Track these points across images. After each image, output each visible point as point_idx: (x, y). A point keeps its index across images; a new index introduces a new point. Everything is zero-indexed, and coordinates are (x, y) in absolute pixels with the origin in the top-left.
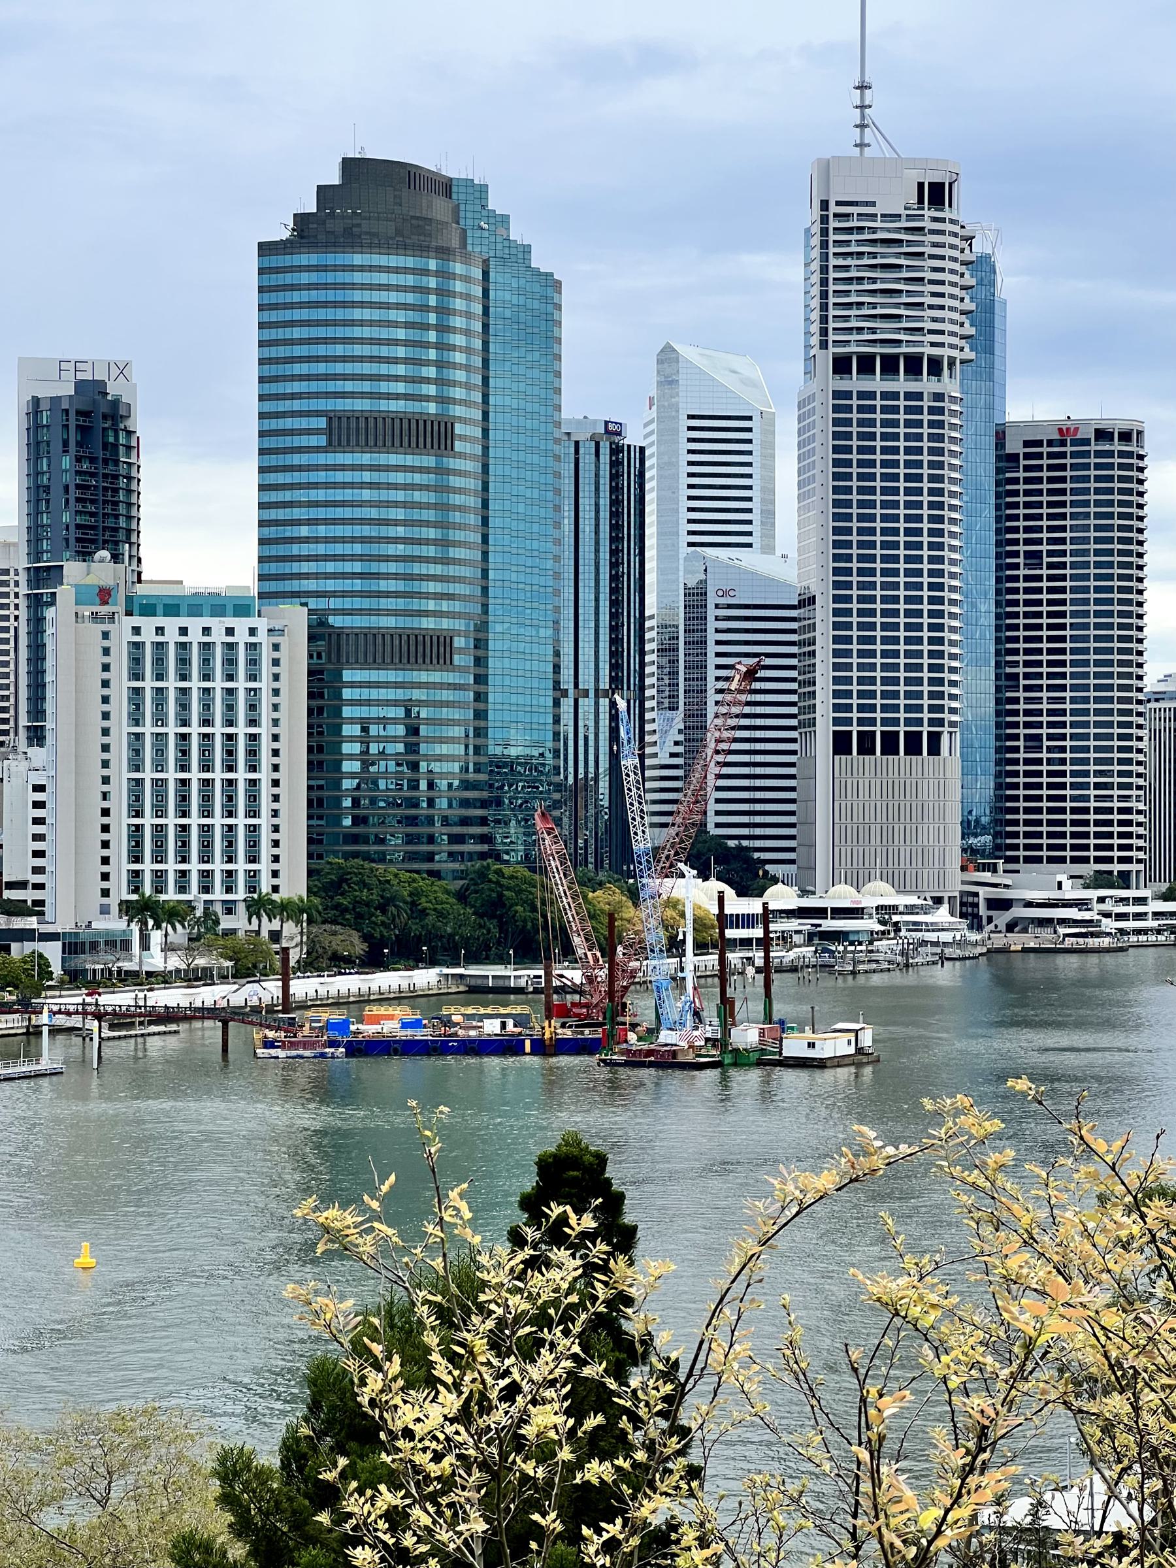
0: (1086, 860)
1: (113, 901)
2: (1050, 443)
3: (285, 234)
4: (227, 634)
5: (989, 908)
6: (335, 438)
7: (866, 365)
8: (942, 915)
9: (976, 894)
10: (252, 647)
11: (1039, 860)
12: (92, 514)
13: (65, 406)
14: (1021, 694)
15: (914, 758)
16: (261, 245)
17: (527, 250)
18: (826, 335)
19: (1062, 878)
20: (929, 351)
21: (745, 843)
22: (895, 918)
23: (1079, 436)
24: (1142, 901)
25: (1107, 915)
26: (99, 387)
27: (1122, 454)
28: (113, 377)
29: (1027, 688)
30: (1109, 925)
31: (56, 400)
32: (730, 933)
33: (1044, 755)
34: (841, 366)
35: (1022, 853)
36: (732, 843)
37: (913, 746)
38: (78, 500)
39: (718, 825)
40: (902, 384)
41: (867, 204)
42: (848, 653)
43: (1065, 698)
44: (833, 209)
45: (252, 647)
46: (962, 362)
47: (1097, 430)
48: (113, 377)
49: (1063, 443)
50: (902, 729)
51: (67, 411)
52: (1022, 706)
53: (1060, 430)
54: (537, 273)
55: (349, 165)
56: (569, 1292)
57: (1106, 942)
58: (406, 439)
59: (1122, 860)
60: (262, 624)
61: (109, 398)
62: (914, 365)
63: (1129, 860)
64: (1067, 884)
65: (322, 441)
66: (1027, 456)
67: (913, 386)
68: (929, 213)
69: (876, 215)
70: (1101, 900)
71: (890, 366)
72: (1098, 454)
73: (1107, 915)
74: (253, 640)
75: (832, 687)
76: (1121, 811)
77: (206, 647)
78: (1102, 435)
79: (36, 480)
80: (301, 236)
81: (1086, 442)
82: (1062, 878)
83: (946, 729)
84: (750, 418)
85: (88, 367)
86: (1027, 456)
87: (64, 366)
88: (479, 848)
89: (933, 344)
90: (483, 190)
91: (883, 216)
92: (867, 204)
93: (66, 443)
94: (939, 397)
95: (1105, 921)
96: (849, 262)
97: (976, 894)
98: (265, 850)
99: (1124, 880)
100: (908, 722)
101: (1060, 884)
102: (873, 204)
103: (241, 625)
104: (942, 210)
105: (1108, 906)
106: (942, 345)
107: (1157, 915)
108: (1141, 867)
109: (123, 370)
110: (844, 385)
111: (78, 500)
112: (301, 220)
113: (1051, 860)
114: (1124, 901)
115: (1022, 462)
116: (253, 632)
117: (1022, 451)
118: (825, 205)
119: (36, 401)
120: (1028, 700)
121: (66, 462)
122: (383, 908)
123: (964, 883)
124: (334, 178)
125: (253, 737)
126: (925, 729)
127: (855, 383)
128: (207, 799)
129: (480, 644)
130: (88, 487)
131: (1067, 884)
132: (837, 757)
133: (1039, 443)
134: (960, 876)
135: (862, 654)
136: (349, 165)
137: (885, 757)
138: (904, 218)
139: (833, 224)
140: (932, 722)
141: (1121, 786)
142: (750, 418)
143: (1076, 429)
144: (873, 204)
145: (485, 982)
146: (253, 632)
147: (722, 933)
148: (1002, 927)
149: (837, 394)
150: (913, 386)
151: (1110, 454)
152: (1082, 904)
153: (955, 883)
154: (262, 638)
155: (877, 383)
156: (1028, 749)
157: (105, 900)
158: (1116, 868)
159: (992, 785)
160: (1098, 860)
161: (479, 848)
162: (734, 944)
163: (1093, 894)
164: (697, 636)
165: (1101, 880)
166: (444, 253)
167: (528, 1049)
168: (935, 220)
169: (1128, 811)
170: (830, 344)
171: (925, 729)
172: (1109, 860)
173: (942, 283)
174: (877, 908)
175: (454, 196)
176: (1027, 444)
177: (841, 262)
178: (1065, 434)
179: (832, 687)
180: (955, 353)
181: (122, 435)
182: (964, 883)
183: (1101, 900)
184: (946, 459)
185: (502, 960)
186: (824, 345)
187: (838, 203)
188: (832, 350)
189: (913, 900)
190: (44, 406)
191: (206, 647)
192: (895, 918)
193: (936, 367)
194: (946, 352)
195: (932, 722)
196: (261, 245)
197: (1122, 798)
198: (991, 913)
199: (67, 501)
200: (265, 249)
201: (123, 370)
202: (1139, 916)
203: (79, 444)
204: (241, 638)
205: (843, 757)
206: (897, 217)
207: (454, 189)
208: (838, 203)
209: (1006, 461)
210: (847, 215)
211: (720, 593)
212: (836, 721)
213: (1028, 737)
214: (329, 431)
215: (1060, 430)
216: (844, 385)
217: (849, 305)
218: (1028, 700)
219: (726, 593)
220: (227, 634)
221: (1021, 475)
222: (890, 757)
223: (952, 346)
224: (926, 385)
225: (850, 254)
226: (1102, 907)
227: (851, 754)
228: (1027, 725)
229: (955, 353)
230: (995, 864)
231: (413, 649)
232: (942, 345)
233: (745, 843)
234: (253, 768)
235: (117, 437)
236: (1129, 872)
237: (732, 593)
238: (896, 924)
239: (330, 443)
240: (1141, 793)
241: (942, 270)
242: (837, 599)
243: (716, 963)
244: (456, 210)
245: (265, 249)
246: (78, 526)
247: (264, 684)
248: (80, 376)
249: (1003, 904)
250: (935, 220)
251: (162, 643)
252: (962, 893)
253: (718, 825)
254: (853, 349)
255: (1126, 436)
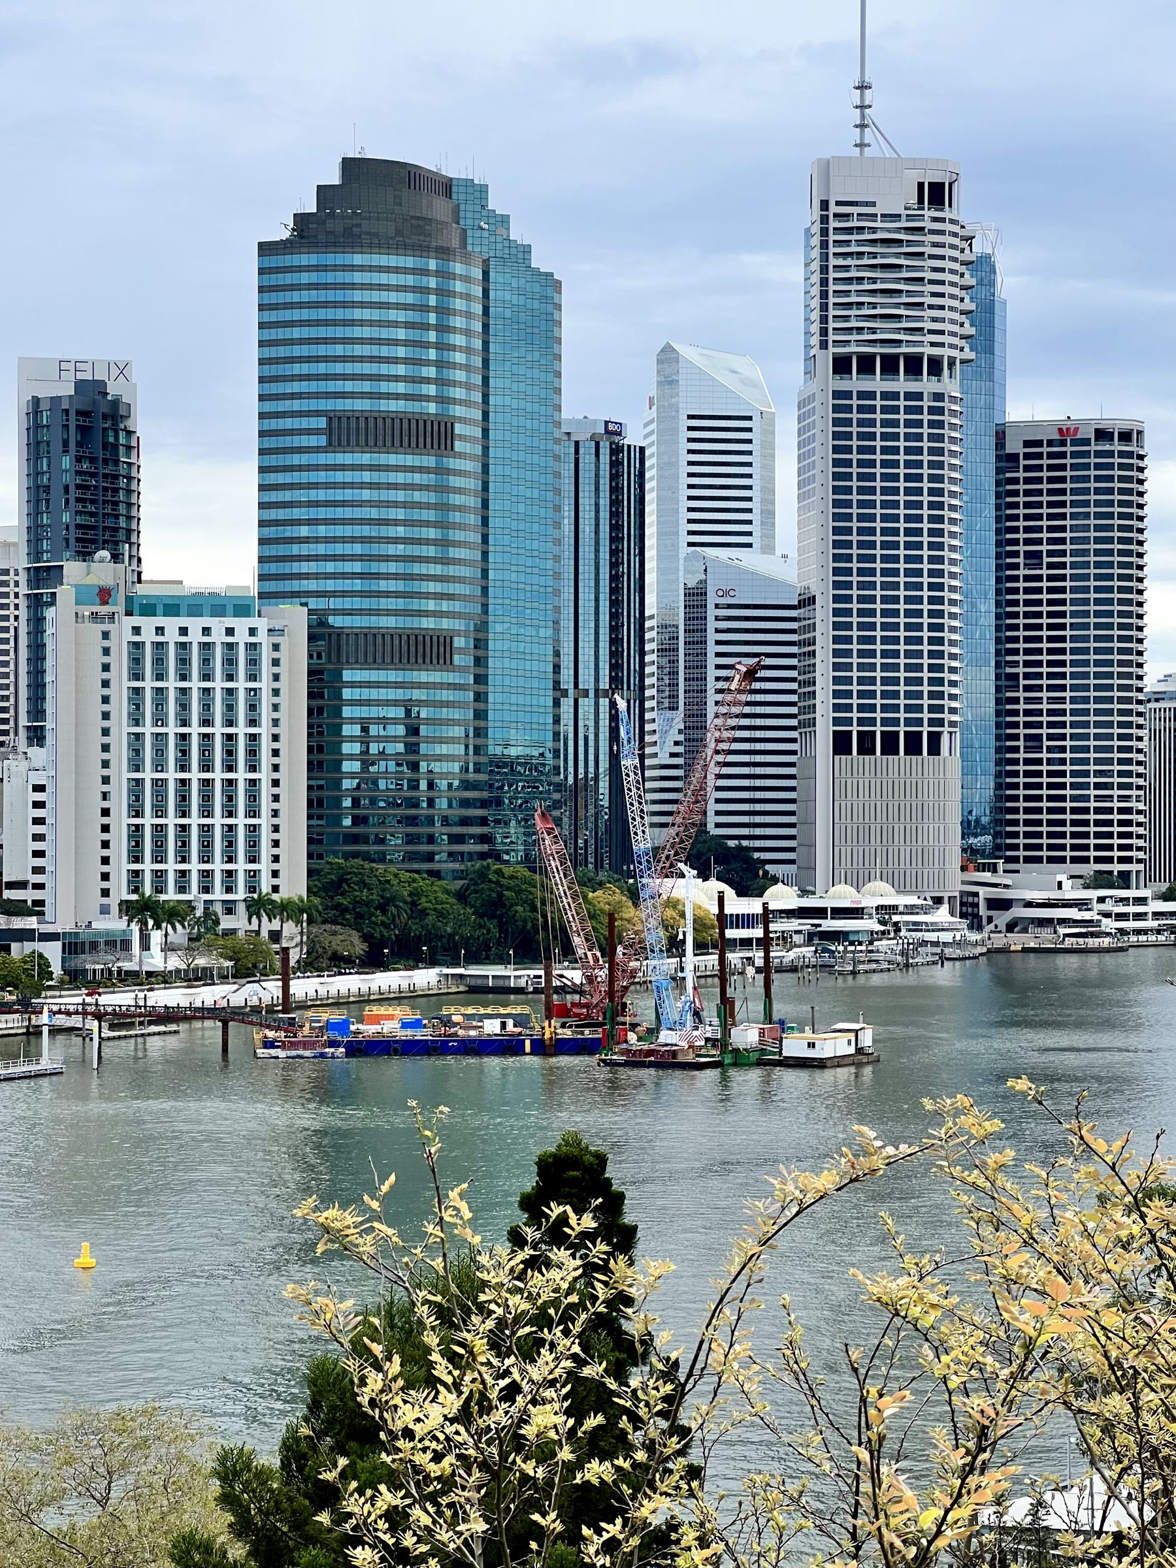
0: (1086, 860)
1: (113, 901)
2: (1050, 443)
3: (285, 234)
4: (227, 634)
5: (989, 908)
6: (335, 438)
7: (866, 365)
8: (942, 915)
9: (976, 894)
10: (252, 647)
11: (1039, 860)
12: (92, 514)
13: (65, 406)
14: (1021, 694)
15: (914, 758)
16: (261, 245)
17: (527, 250)
18: (826, 335)
19: (1062, 878)
20: (929, 351)
21: (745, 843)
22: (895, 918)
23: (1079, 436)
24: (1142, 901)
25: (1107, 915)
26: (99, 387)
27: (1122, 454)
28: (113, 377)
29: (1027, 688)
30: (1109, 925)
31: (56, 400)
32: (730, 933)
33: (1044, 755)
34: (841, 366)
35: (1022, 853)
36: (732, 843)
37: (913, 746)
38: (78, 500)
39: (718, 825)
40: (902, 384)
41: (867, 204)
42: (848, 653)
43: (1065, 698)
44: (833, 209)
45: (252, 647)
46: (962, 362)
47: (1097, 430)
48: (113, 377)
49: (1063, 443)
50: (902, 729)
51: (67, 411)
52: (1022, 706)
53: (1060, 430)
54: (537, 273)
55: (349, 165)
56: (569, 1292)
57: (1106, 942)
58: (406, 439)
59: (1122, 860)
60: (262, 624)
61: (109, 398)
62: (914, 365)
63: (1129, 860)
64: (1067, 884)
65: (322, 441)
66: (1027, 456)
67: (913, 386)
68: (929, 213)
69: (876, 215)
70: (1101, 900)
71: (890, 366)
72: (1098, 454)
73: (1107, 915)
74: (253, 640)
75: (832, 687)
76: (1121, 811)
77: (206, 647)
78: (1102, 435)
79: (36, 480)
80: (301, 236)
81: (1086, 442)
82: (1062, 878)
83: (946, 729)
84: (750, 418)
85: (88, 367)
86: (1027, 456)
87: (64, 366)
88: (479, 848)
89: (933, 344)
90: (483, 190)
91: (883, 216)
92: (867, 204)
93: (66, 443)
94: (939, 397)
95: (1105, 921)
96: (849, 262)
97: (976, 894)
98: (265, 850)
99: (1124, 880)
100: (908, 722)
101: (1060, 884)
102: (873, 204)
103: (241, 625)
104: (942, 210)
105: (1108, 906)
106: (942, 345)
107: (1157, 915)
108: (1141, 867)
109: (123, 370)
110: (844, 385)
111: (78, 500)
112: (301, 220)
113: (1051, 860)
114: (1124, 901)
115: (1022, 462)
116: (253, 632)
117: (1022, 451)
118: (825, 205)
119: (36, 401)
120: (1028, 700)
121: (66, 462)
122: (383, 908)
123: (964, 883)
124: (334, 178)
125: (253, 737)
126: (925, 729)
127: (855, 383)
128: (207, 799)
129: (480, 644)
130: (88, 487)
131: (1067, 884)
132: (837, 757)
133: (1039, 443)
134: (960, 876)
135: (862, 654)
136: (349, 165)
137: (885, 757)
138: (904, 218)
139: (833, 224)
140: (932, 722)
141: (1121, 786)
142: (750, 418)
143: (1076, 429)
144: (873, 204)
145: (485, 982)
146: (253, 632)
147: (722, 933)
148: (1002, 927)
149: (837, 394)
150: (913, 386)
151: (1110, 454)
152: (1082, 904)
153: (955, 883)
154: (262, 638)
155: (877, 383)
156: (1028, 749)
157: (105, 900)
158: (1116, 868)
159: (992, 785)
160: (1098, 860)
161: (479, 848)
162: (734, 944)
163: (1093, 894)
164: (697, 636)
165: (1101, 880)
166: (444, 253)
167: (528, 1049)
168: (935, 220)
169: (1128, 811)
170: (830, 344)
171: (925, 729)
172: (1109, 860)
173: (942, 283)
174: (877, 908)
175: (454, 196)
176: (1027, 444)
177: (841, 262)
178: (1065, 434)
179: (832, 687)
180: (955, 353)
181: (122, 435)
182: (964, 883)
183: (1101, 900)
184: (946, 459)
185: (502, 960)
186: (824, 345)
187: (838, 203)
188: (832, 350)
189: (913, 900)
190: (44, 406)
191: (206, 647)
192: (895, 918)
193: (936, 367)
194: (946, 352)
195: (932, 722)
196: (261, 245)
197: (1122, 798)
198: (991, 913)
199: (67, 501)
200: (265, 249)
201: (123, 370)
202: (1139, 916)
203: (79, 444)
204: (241, 638)
205: (843, 757)
206: (897, 217)
207: (454, 189)
208: (838, 203)
209: (1006, 461)
210: (847, 215)
211: (720, 593)
212: (836, 721)
213: (1028, 737)
214: (329, 431)
215: (1060, 430)
216: (844, 385)
217: (849, 305)
218: (1028, 700)
219: (726, 593)
220: (227, 634)
221: (1021, 475)
222: (890, 757)
223: (952, 346)
224: (926, 385)
225: (850, 254)
226: (1102, 907)
227: (851, 754)
228: (1027, 725)
229: (955, 353)
230: (995, 864)
231: (413, 649)
232: (942, 345)
233: (745, 843)
234: (253, 768)
235: (117, 437)
236: (1129, 872)
237: (732, 593)
238: (896, 924)
239: (330, 443)
240: (1141, 793)
241: (942, 270)
242: (837, 599)
243: (716, 963)
244: (456, 210)
245: (265, 249)
246: (78, 526)
247: (264, 684)
248: (80, 376)
249: (1003, 904)
250: (935, 220)
251: (162, 643)
252: (962, 893)
253: (718, 825)
254: (853, 349)
255: (1126, 436)
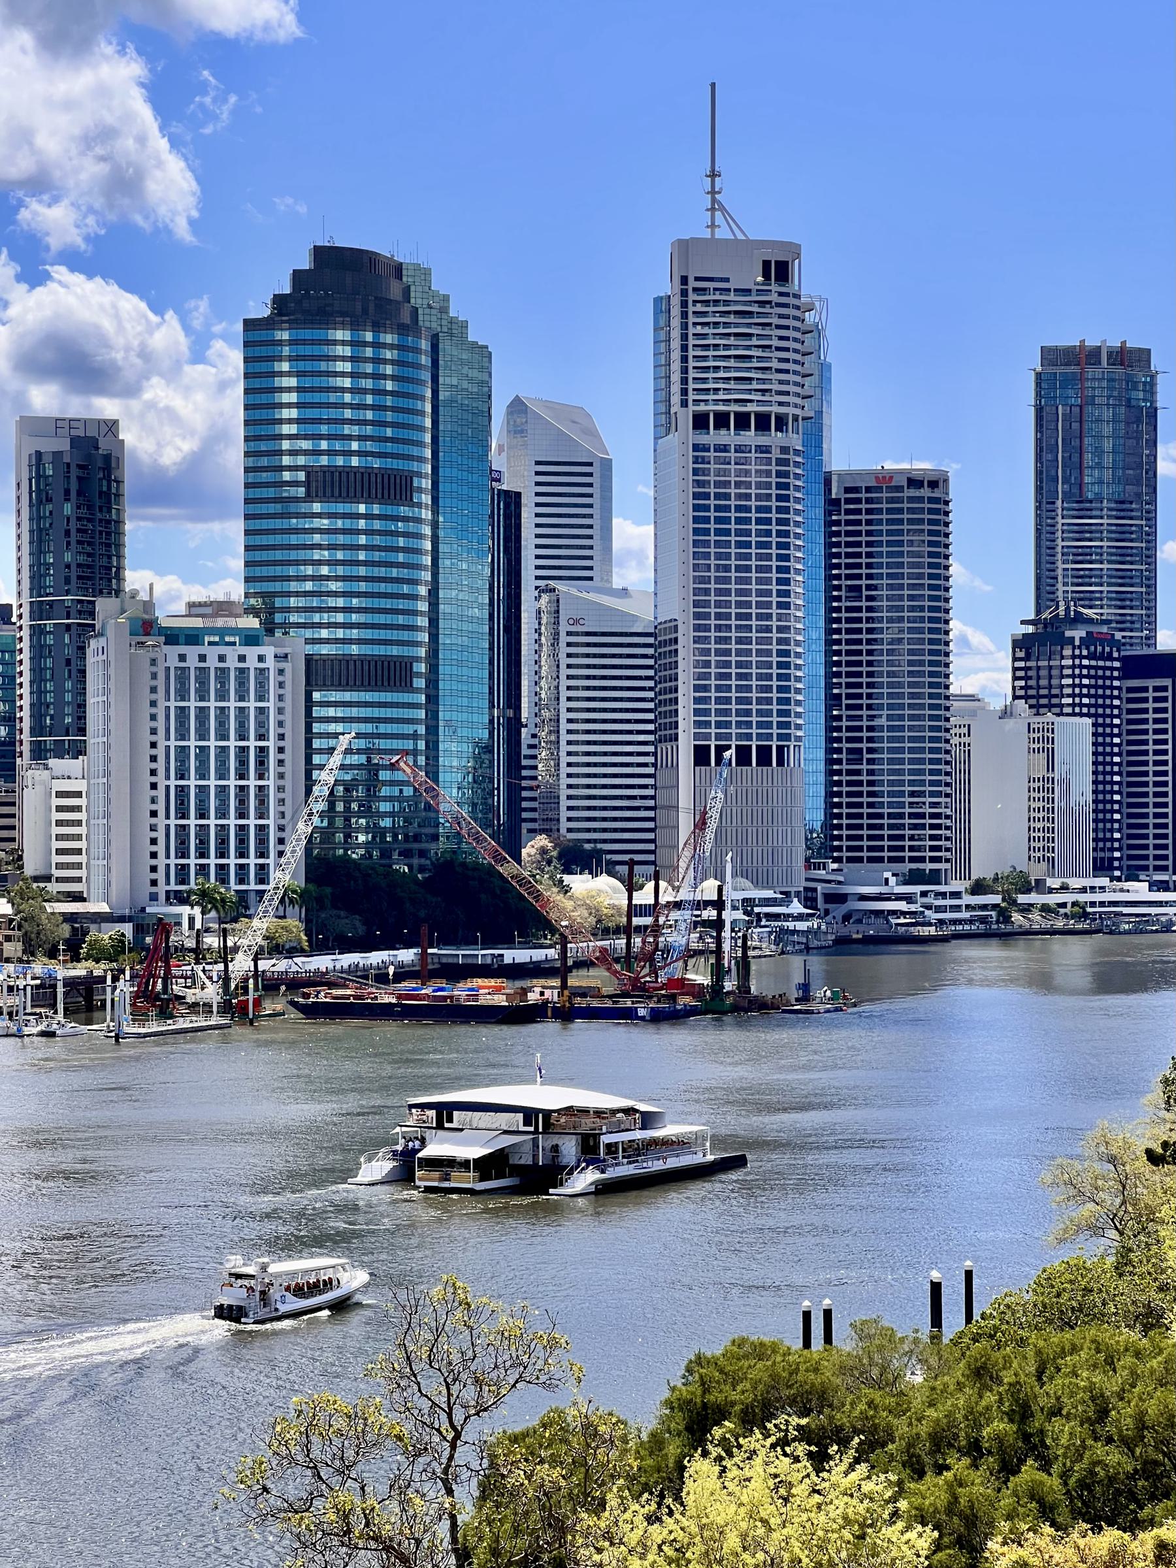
2: (868, 489)
3: (266, 312)
4: (240, 661)
5: (826, 902)
6: (313, 490)
7: (722, 420)
8: (796, 907)
9: (815, 890)
10: (262, 672)
11: (860, 860)
12: (89, 555)
13: (67, 459)
14: (844, 713)
15: (765, 768)
17: (464, 325)
18: (686, 395)
19: (887, 875)
20: (775, 409)
21: (599, 846)
22: (757, 910)
23: (893, 484)
24: (956, 895)
25: (929, 907)
26: (94, 443)
28: (102, 434)
31: (57, 455)
32: (636, 921)
34: (700, 422)
36: (587, 846)
38: (79, 542)
39: (569, 830)
43: (861, 716)
44: (692, 284)
46: (803, 419)
48: (102, 434)
49: (879, 489)
51: (68, 465)
53: (877, 478)
54: (475, 344)
55: (322, 254)
57: (932, 930)
59: (933, 860)
60: (269, 651)
61: (100, 452)
66: (848, 501)
67: (763, 440)
68: (774, 287)
69: (729, 290)
70: (924, 894)
71: (742, 422)
72: (911, 499)
73: (929, 907)
74: (262, 665)
79: (38, 524)
80: (280, 314)
81: (899, 489)
83: (792, 744)
87: (59, 424)
89: (780, 404)
90: (427, 273)
91: (736, 290)
93: (67, 492)
94: (784, 450)
95: (927, 912)
96: (706, 330)
97: (815, 890)
99: (934, 878)
101: (887, 880)
102: (727, 280)
103: (252, 652)
106: (788, 404)
107: (968, 907)
108: (948, 866)
110: (703, 439)
111: (79, 542)
112: (279, 301)
113: (871, 860)
114: (943, 895)
115: (844, 507)
116: (261, 658)
117: (843, 496)
118: (684, 280)
119: (39, 454)
123: (807, 880)
124: (306, 264)
126: (774, 744)
127: (714, 437)
128: (242, 802)
129: (433, 668)
131: (893, 881)
132: (698, 768)
137: (739, 768)
138: (754, 293)
143: (891, 478)
144: (727, 280)
145: (455, 961)
146: (261, 658)
148: (839, 919)
149: (696, 448)
150: (763, 440)
152: (909, 899)
154: (270, 663)
156: (849, 761)
157: (154, 889)
158: (929, 866)
159: (823, 794)
160: (913, 860)
162: (639, 929)
163: (917, 889)
165: (914, 878)
167: (549, 1014)
170: (690, 403)
171: (774, 744)
174: (743, 900)
175: (404, 279)
176: (848, 490)
177: (699, 329)
178: (884, 481)
180: (798, 411)
182: (807, 880)
183: (924, 894)
184: (792, 504)
185: (470, 942)
186: (684, 404)
187: (697, 279)
188: (692, 408)
190: (47, 459)
192: (757, 910)
194: (791, 411)
198: (828, 906)
199: (68, 543)
200: (249, 324)
202: (957, 908)
203: (79, 493)
204: (252, 663)
205: (703, 768)
206: (748, 291)
207: (404, 272)
208: (697, 279)
209: (832, 505)
210: (704, 289)
211: (571, 622)
212: (697, 736)
213: (849, 751)
214: (307, 484)
215: (877, 478)
216: (703, 439)
219: (576, 622)
220: (240, 661)
222: (744, 768)
224: (775, 438)
225: (707, 324)
227: (709, 765)
229: (798, 411)
230: (824, 863)
231: (379, 672)
232: (788, 404)
233: (599, 846)
236: (939, 871)
237: (581, 622)
239: (308, 493)
240: (948, 800)
241: (787, 339)
242: (697, 628)
243: (624, 946)
246: (79, 565)
247: (271, 704)
251: (264, 669)
252: (805, 888)
253: (569, 830)
254: (711, 407)
255: (933, 484)
